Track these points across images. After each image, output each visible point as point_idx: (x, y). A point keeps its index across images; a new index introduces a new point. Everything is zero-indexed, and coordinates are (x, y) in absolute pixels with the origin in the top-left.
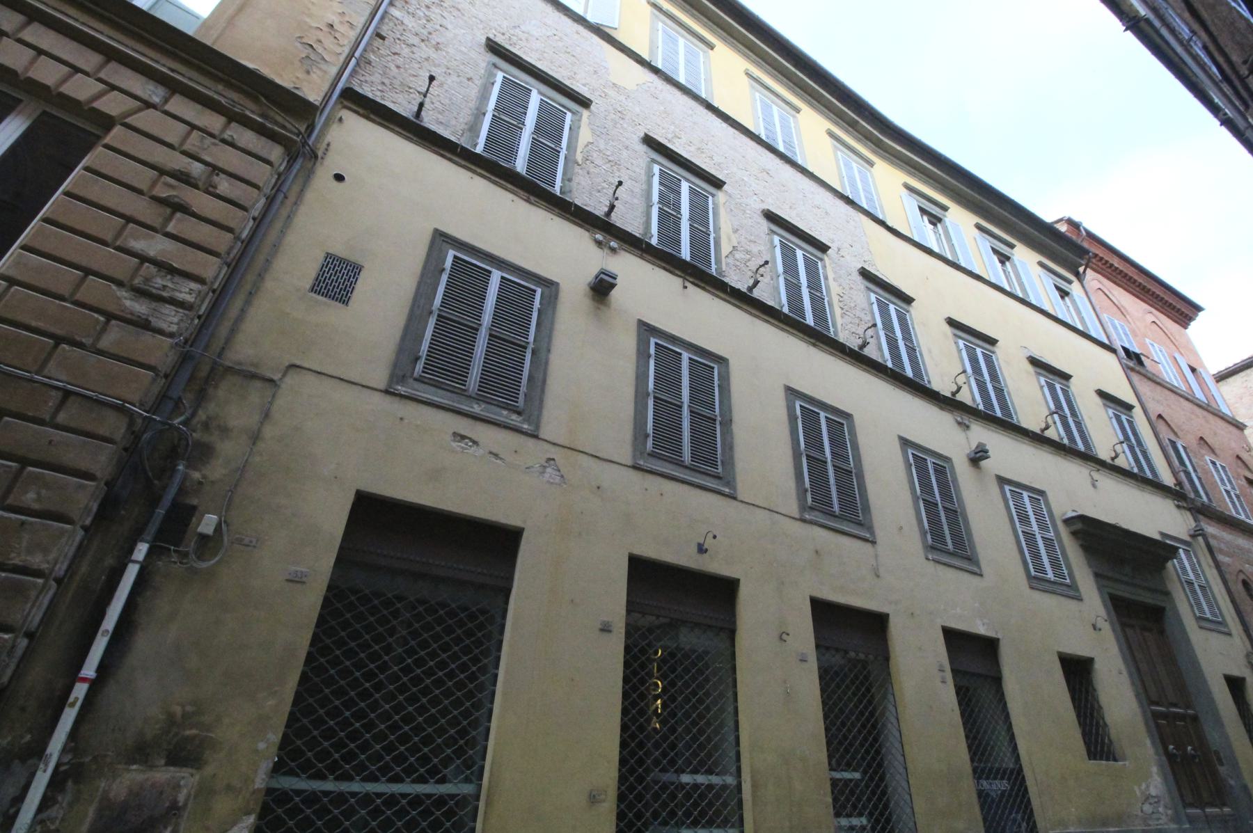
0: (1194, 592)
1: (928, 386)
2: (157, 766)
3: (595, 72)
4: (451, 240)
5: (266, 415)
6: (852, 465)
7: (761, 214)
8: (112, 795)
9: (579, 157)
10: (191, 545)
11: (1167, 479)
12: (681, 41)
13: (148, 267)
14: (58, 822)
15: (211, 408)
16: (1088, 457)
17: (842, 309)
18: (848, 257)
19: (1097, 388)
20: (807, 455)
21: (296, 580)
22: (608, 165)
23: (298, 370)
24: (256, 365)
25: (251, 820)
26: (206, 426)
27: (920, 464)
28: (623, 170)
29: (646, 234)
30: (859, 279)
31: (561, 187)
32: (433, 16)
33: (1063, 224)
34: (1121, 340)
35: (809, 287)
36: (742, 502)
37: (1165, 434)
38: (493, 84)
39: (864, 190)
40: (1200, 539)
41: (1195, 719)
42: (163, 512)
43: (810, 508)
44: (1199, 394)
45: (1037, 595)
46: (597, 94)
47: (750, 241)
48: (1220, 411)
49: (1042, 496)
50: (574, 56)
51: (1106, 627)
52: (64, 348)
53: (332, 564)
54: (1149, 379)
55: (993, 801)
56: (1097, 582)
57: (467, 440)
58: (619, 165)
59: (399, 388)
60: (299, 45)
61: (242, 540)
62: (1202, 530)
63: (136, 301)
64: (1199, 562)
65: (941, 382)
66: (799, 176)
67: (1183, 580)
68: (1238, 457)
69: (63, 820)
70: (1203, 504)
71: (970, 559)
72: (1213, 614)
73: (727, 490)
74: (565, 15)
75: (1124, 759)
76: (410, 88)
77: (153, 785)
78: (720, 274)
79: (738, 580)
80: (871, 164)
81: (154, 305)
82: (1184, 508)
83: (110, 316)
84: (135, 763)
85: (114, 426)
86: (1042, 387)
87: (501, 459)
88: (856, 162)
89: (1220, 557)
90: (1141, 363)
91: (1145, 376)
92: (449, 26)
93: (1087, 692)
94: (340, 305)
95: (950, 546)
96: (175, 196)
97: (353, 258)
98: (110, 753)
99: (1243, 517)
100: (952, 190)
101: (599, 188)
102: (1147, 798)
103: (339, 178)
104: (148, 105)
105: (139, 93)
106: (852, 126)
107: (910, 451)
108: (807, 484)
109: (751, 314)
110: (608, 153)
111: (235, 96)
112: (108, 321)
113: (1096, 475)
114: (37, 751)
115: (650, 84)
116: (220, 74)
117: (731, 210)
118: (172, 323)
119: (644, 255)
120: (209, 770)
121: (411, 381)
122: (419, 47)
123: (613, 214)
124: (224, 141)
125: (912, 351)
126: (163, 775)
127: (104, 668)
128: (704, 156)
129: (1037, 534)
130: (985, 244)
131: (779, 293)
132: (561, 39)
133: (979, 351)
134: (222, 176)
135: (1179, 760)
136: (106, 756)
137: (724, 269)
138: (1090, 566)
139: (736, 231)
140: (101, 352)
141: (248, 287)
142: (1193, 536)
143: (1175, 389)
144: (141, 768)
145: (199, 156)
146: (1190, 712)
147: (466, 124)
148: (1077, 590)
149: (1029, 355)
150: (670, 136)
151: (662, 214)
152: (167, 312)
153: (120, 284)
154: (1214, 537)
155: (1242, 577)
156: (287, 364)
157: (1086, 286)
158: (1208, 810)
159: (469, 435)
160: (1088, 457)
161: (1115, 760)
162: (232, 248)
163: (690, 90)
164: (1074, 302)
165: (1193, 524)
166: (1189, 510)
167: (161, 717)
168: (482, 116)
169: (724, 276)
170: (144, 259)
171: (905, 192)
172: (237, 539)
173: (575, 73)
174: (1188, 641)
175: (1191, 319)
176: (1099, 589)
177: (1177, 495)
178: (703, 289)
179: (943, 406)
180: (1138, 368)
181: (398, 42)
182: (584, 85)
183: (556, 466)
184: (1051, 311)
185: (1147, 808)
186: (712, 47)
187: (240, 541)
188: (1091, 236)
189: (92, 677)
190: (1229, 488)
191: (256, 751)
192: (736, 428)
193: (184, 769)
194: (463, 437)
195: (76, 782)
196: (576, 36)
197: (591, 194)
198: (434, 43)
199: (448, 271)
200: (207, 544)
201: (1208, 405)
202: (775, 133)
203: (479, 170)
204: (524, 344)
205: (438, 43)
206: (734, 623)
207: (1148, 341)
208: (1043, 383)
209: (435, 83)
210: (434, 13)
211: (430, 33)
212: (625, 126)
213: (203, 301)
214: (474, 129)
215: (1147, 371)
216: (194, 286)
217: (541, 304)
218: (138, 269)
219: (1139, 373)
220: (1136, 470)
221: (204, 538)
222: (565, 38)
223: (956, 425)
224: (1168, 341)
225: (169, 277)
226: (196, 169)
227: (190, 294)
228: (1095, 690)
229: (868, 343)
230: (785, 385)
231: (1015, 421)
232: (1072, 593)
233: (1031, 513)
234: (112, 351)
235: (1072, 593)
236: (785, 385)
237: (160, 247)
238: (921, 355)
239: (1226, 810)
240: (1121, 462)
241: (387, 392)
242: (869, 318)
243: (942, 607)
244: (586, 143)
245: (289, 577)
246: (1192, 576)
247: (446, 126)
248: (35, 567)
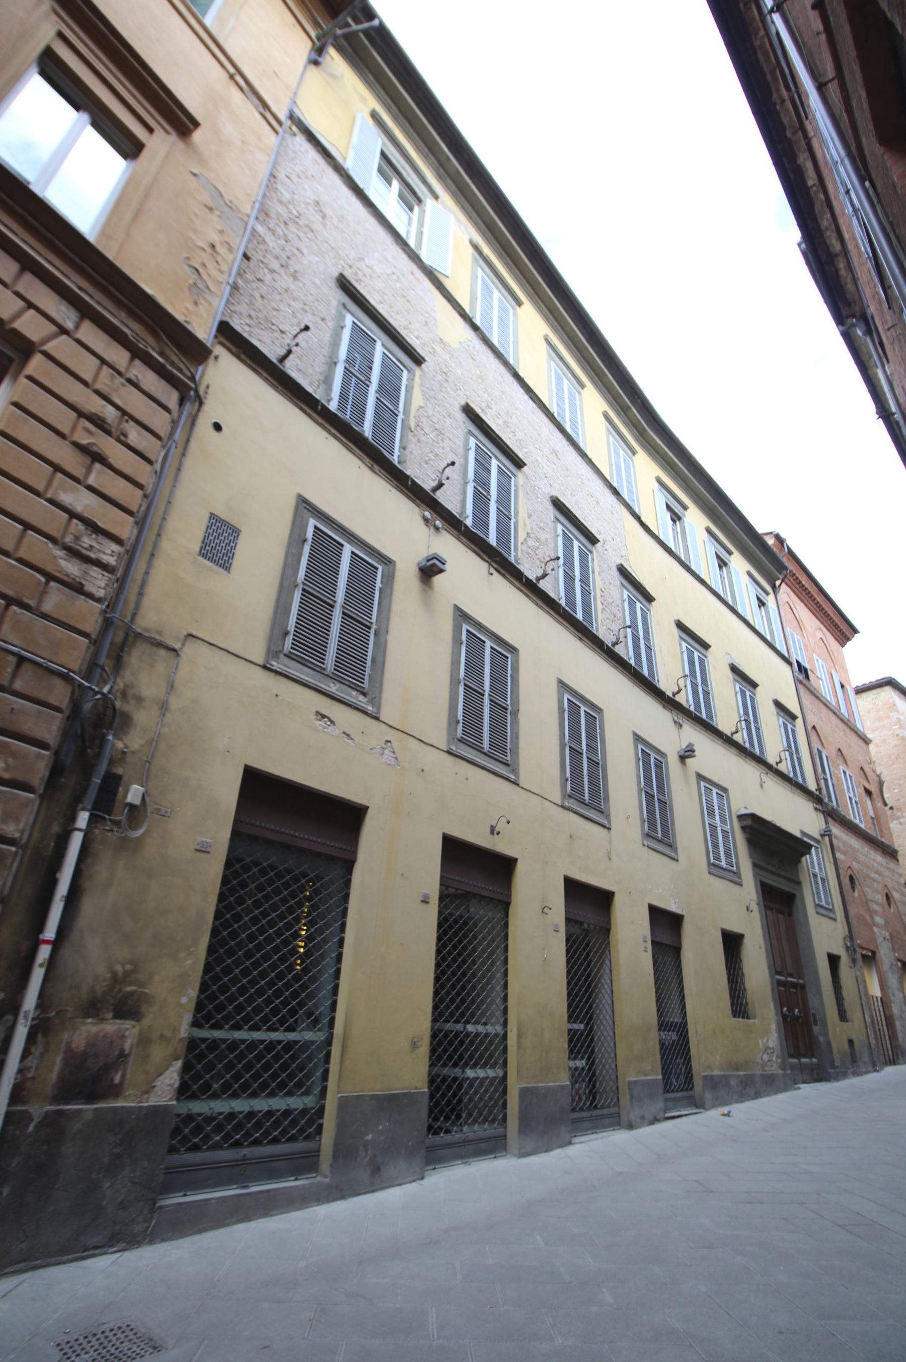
0: (816, 883)
1: (595, 632)
2: (106, 1019)
3: (426, 323)
4: (312, 507)
5: (171, 687)
6: (600, 758)
7: (549, 500)
8: (74, 1045)
9: (412, 423)
10: (121, 816)
11: (812, 785)
12: (496, 294)
13: (77, 524)
14: (33, 1070)
15: (127, 674)
16: (760, 761)
17: (603, 604)
18: (610, 551)
19: (774, 698)
20: (570, 747)
21: (203, 850)
22: (434, 434)
23: (195, 639)
24: (160, 633)
25: (179, 1064)
26: (124, 694)
27: (475, 645)
28: (446, 441)
29: (462, 514)
30: (616, 573)
31: (399, 456)
32: (290, 236)
33: (771, 538)
34: (796, 653)
35: (498, 502)
36: (522, 788)
37: (816, 745)
38: (342, 328)
39: (627, 481)
40: (827, 838)
41: (803, 987)
42: (99, 781)
43: (569, 796)
44: (843, 710)
45: (713, 879)
46: (427, 349)
47: (540, 528)
48: (856, 726)
49: (725, 792)
50: (408, 301)
51: (754, 907)
52: (15, 611)
53: (229, 836)
54: (811, 692)
55: (666, 1048)
56: (754, 871)
57: (326, 719)
58: (443, 434)
59: (275, 663)
60: (186, 267)
61: (160, 810)
62: (830, 831)
63: (69, 562)
64: (823, 857)
65: (666, 685)
66: (579, 459)
67: (811, 873)
68: (862, 768)
69: (37, 1069)
70: (833, 808)
71: (671, 846)
72: (827, 903)
73: (513, 777)
74: (403, 250)
75: (754, 1018)
76: (273, 324)
77: (105, 1036)
78: (516, 561)
79: (515, 860)
80: (582, 386)
81: (84, 566)
82: (820, 810)
83: (50, 577)
84: (89, 1017)
85: (60, 694)
86: (736, 693)
87: (352, 739)
88: (482, 269)
89: (838, 855)
90: (807, 677)
91: (808, 689)
92: (305, 251)
93: (736, 961)
94: (220, 570)
95: (660, 835)
96: (93, 444)
97: (233, 521)
98: (69, 1009)
99: (857, 821)
100: (697, 495)
101: (427, 458)
102: (767, 1049)
103: (217, 427)
104: (63, 331)
105: (54, 314)
106: (623, 411)
107: (465, 627)
108: (568, 775)
109: (537, 604)
110: (435, 420)
111: (136, 326)
112: (47, 582)
113: (764, 777)
114: (14, 1007)
115: (469, 343)
116: (125, 300)
117: (527, 493)
118: (99, 587)
119: (461, 536)
120: (147, 1021)
121: (282, 656)
122: (279, 274)
123: (438, 492)
124: (129, 381)
125: (586, 593)
126: (111, 1027)
127: (61, 931)
128: (509, 430)
129: (718, 826)
130: (711, 548)
131: (558, 584)
132: (398, 280)
133: (696, 654)
134: (132, 423)
135: (789, 1020)
136: (67, 1011)
137: (519, 557)
138: (751, 856)
139: (530, 516)
140: (45, 616)
141: (149, 548)
142: (822, 836)
143: (827, 703)
144: (95, 1021)
145: (110, 397)
146: (801, 981)
147: (321, 374)
148: (740, 877)
149: (731, 662)
150: (484, 405)
151: (477, 493)
152: (95, 575)
153: (53, 540)
154: (836, 837)
155: (850, 872)
156: (185, 633)
157: (778, 598)
158: (803, 1060)
159: (328, 715)
160: (760, 761)
161: (748, 1018)
162: (141, 506)
163: (502, 355)
164: (767, 613)
165: (824, 826)
166: (823, 812)
167: (109, 975)
168: (333, 365)
169: (519, 564)
170: (73, 515)
171: (656, 486)
172: (156, 809)
173: (410, 323)
174: (807, 923)
175: (848, 639)
176: (754, 876)
177: (816, 798)
178: (503, 576)
179: (666, 705)
180: (805, 681)
181: (261, 264)
182: (417, 338)
183: (392, 748)
184: (751, 622)
185: (766, 1057)
186: (582, 386)
187: (158, 811)
188: (791, 553)
189: (52, 939)
190: (852, 795)
191: (180, 1005)
192: (521, 716)
193: (127, 1022)
194: (324, 716)
195: (45, 1035)
196: (410, 277)
197: (420, 465)
198: (292, 270)
199: (309, 542)
200: (135, 813)
201: (848, 720)
202: (564, 410)
203: (333, 431)
204: (368, 624)
205: (296, 271)
206: (510, 896)
207: (815, 656)
208: (738, 689)
209: (305, 333)
210: (291, 232)
211: (288, 258)
212: (449, 389)
213: (120, 564)
214: (328, 381)
215: (811, 685)
216: (115, 547)
217: (382, 583)
219: (805, 686)
220: (791, 775)
221: (132, 807)
222: (402, 279)
223: (673, 723)
224: (829, 658)
225: (94, 536)
226: (110, 413)
227: (113, 556)
228: (741, 961)
229: (443, 484)
230: (558, 678)
231: (714, 724)
232: (736, 879)
233: (716, 808)
234: (54, 615)
235: (736, 879)
236: (558, 678)
237: (85, 502)
238: (655, 654)
239: (814, 1060)
240: (782, 767)
241: (265, 667)
242: (620, 615)
243: (650, 887)
244: (418, 407)
245: (198, 848)
246: (817, 870)
247: (305, 375)
248: (10, 836)
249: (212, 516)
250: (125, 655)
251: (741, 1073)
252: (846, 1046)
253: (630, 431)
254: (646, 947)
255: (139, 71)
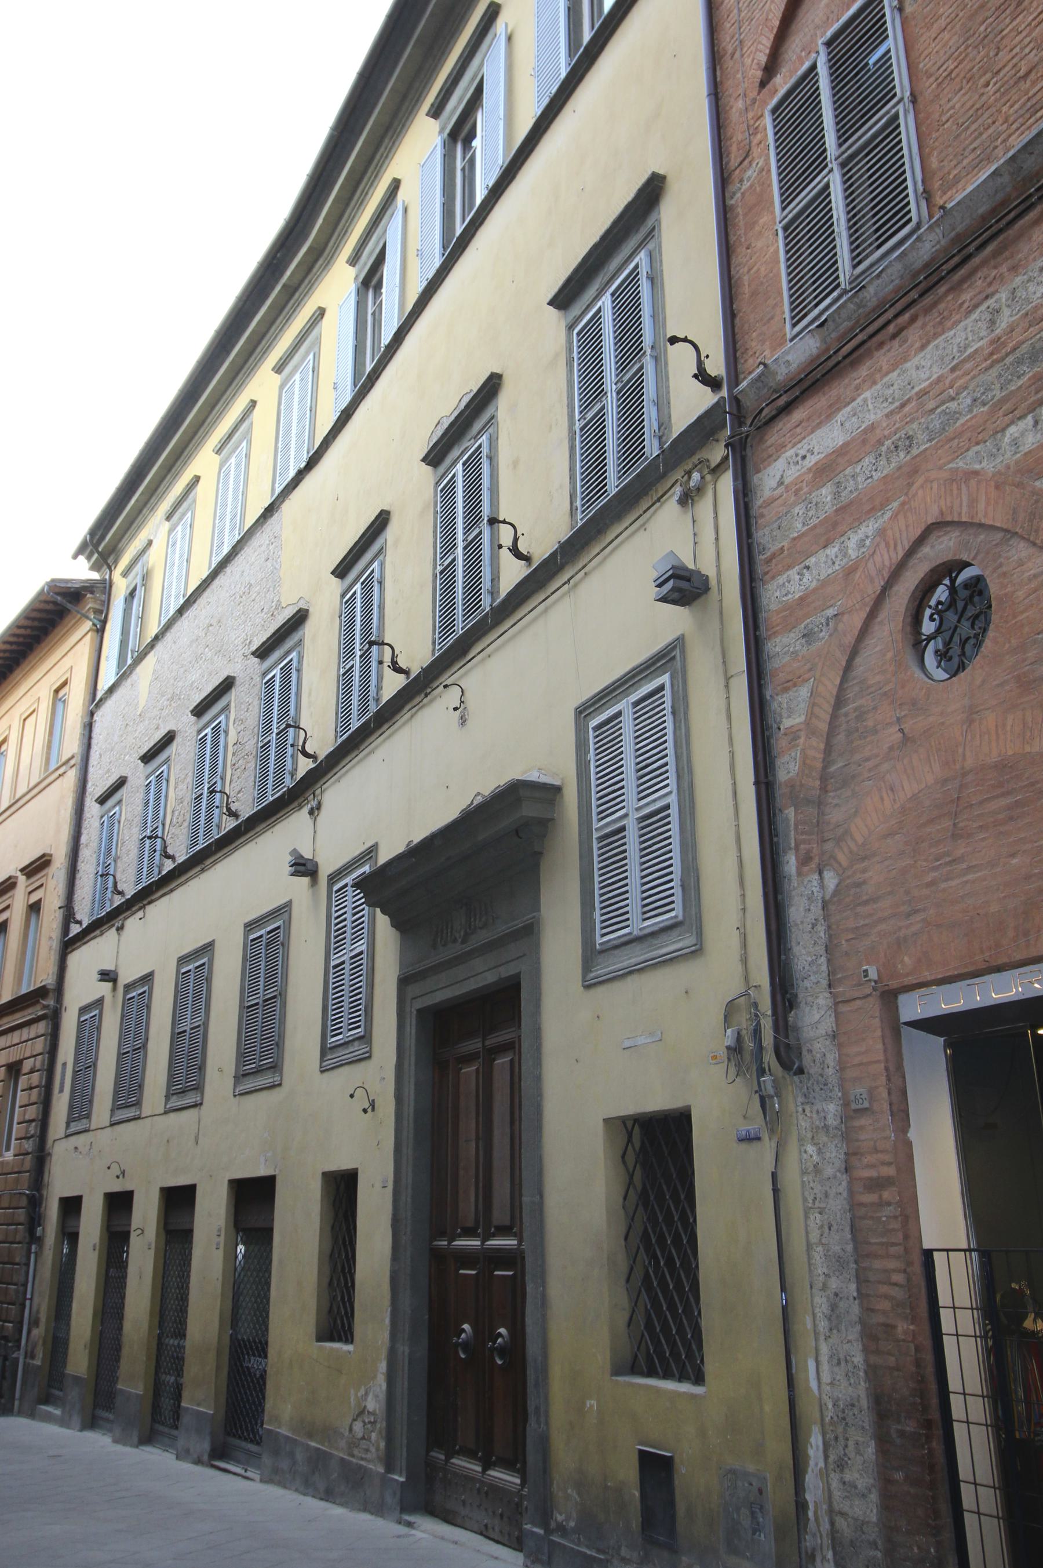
218: (30, 1095)
249: (550, 303)
250: (771, 778)
251: (313, 1444)
252: (628, 1473)
253: (352, 220)
254: (218, 1244)
255: (197, 401)
